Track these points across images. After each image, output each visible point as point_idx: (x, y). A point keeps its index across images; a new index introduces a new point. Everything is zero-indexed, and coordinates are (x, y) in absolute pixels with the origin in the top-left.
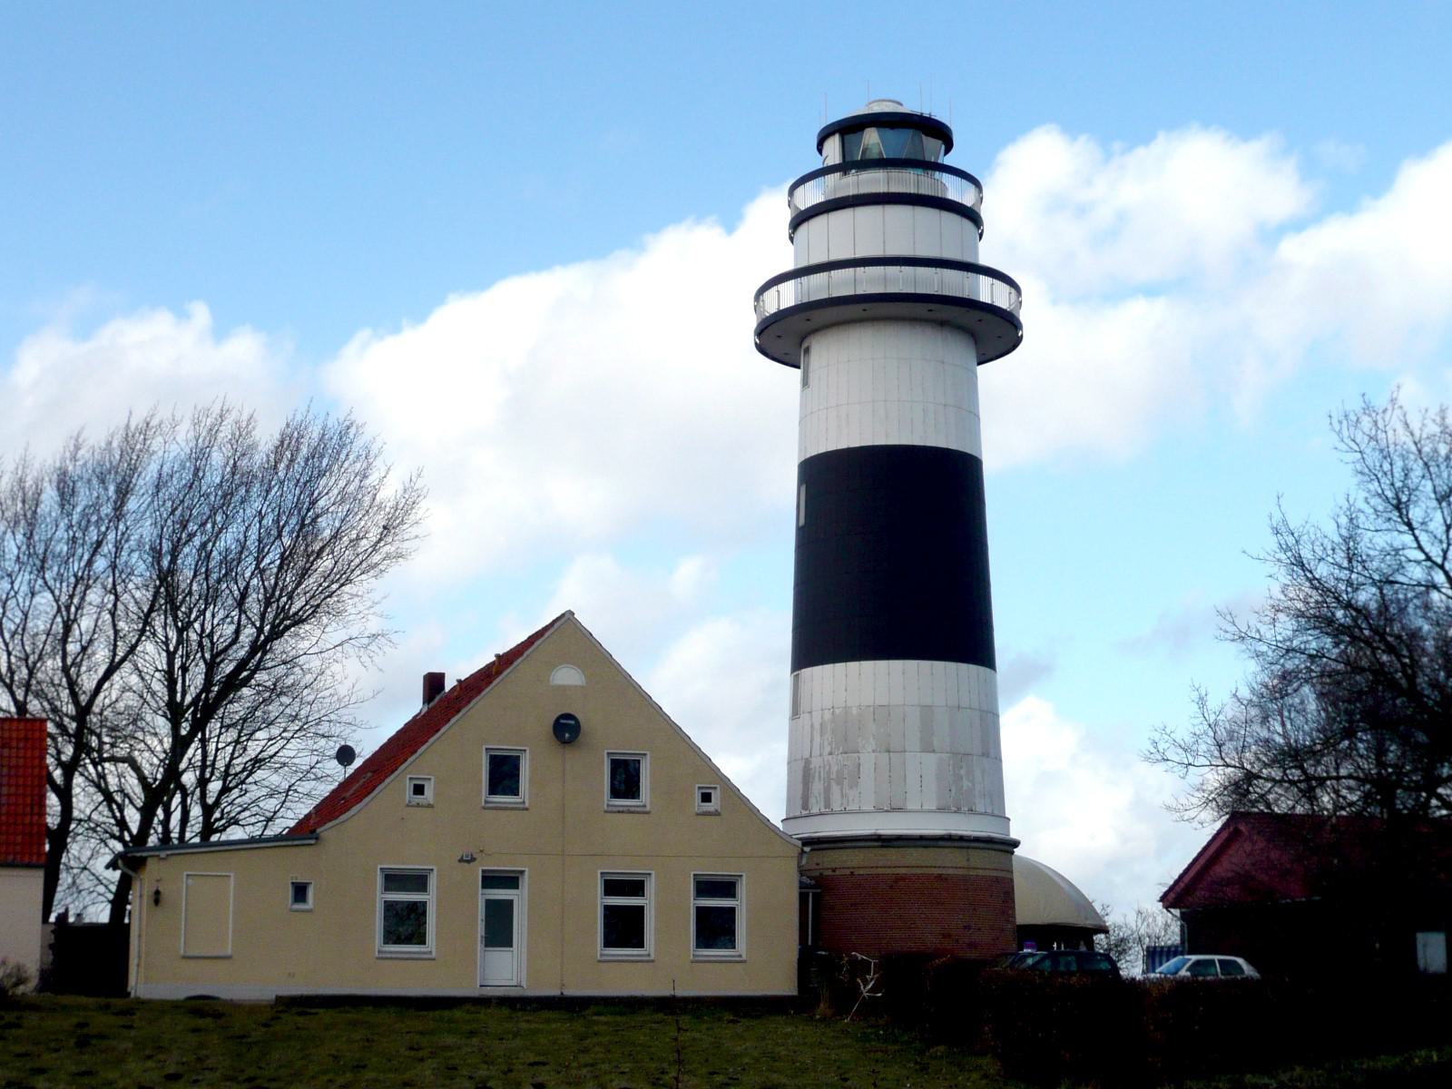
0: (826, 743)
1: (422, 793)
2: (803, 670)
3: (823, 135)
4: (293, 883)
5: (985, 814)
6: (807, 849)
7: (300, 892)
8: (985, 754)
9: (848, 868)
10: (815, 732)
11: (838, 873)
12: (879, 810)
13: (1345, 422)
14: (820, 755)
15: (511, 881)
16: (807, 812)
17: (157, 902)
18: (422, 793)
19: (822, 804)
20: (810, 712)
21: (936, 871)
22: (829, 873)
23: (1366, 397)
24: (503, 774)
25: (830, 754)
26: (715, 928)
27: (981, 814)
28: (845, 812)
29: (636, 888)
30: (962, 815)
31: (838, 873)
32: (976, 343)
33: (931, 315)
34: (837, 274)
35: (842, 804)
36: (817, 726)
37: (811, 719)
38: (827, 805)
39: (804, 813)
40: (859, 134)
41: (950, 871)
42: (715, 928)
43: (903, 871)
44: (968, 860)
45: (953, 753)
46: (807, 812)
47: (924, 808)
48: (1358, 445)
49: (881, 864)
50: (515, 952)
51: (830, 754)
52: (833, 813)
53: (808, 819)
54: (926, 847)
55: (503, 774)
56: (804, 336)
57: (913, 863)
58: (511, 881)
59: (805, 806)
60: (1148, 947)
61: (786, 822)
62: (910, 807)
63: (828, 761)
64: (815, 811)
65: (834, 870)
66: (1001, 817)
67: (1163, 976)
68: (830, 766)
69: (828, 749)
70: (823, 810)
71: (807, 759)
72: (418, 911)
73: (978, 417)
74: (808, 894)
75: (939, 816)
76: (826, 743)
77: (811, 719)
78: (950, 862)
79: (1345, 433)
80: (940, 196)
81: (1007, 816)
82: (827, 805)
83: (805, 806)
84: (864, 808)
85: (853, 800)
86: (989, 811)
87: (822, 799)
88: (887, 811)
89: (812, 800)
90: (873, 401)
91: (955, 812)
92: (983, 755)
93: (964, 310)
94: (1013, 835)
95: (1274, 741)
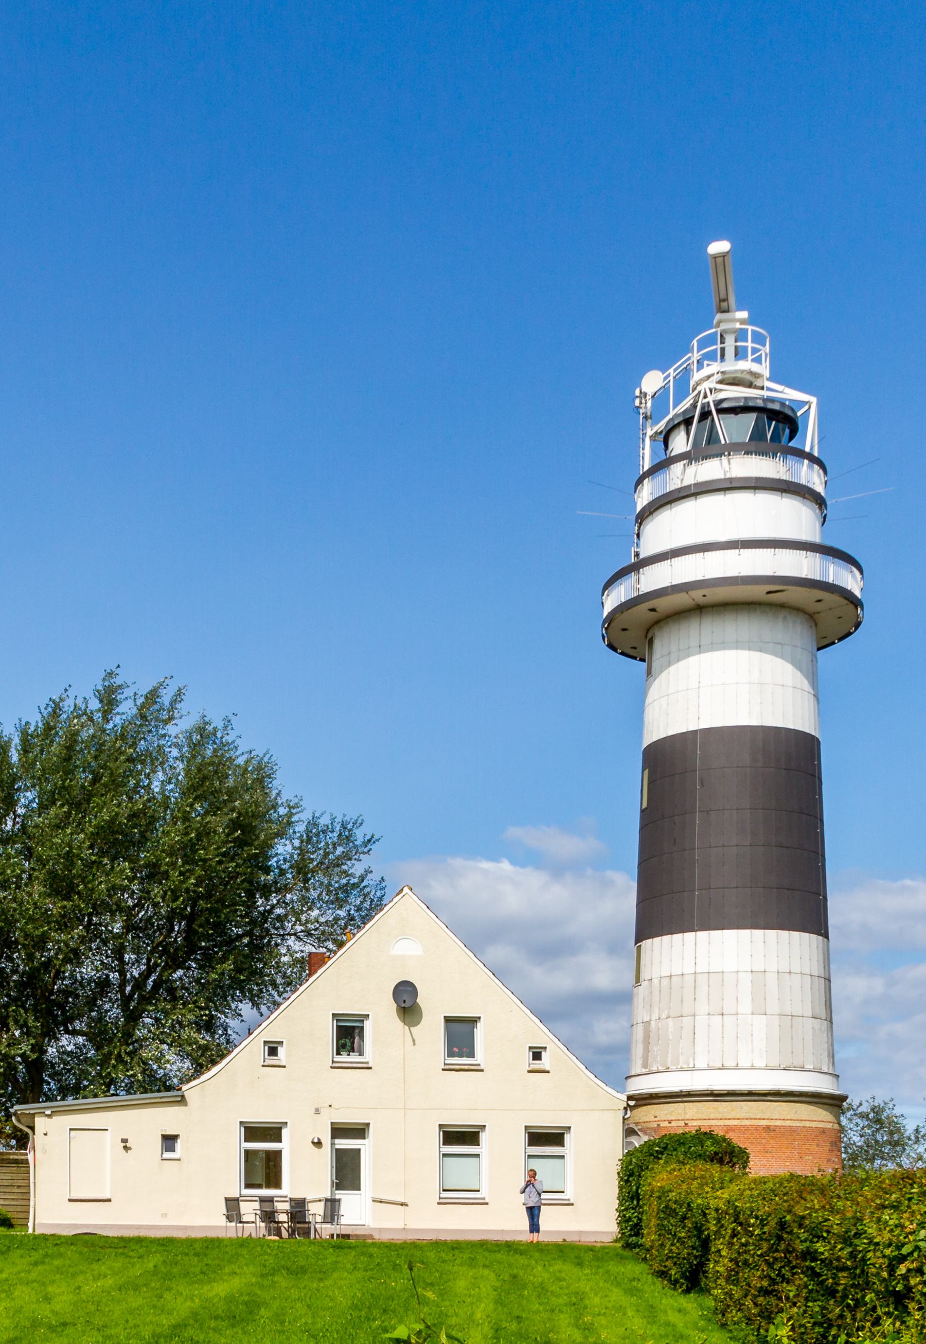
1: (540, 1059)
4: (368, 1124)
6: (632, 1103)
7: (169, 1141)
11: (674, 1124)
15: (360, 1131)
17: (126, 1148)
18: (540, 1059)
24: (348, 1035)
31: (674, 1124)
33: (703, 592)
39: (644, 1071)
41: (778, 1123)
49: (712, 1116)
50: (363, 1195)
55: (348, 1035)
57: (743, 1115)
58: (360, 1131)
60: (683, 1275)
64: (654, 1069)
72: (274, 1159)
80: (831, 581)
93: (700, 555)
95: (20, 760)
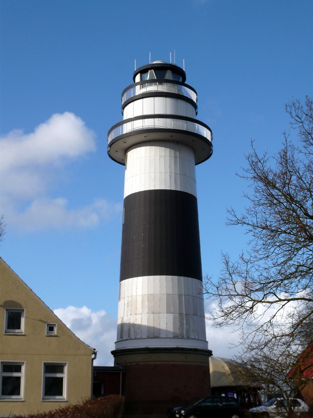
0: (129, 311)
2: (122, 281)
3: (135, 74)
5: (195, 339)
8: (195, 314)
9: (136, 362)
10: (125, 306)
12: (149, 338)
13: (293, 107)
14: (127, 316)
16: (122, 339)
19: (127, 336)
20: (124, 298)
21: (172, 363)
22: (129, 364)
23: (308, 97)
25: (131, 315)
26: (53, 387)
27: (193, 339)
28: (136, 339)
29: (18, 368)
30: (184, 339)
32: (195, 153)
34: (136, 122)
35: (135, 335)
36: (126, 304)
37: (124, 301)
38: (129, 336)
39: (121, 339)
40: (147, 73)
41: (178, 363)
42: (53, 387)
43: (158, 363)
44: (186, 358)
45: (180, 314)
46: (122, 339)
47: (167, 336)
48: (301, 119)
51: (131, 315)
52: (131, 339)
53: (122, 342)
54: (168, 353)
56: (126, 150)
59: (121, 337)
61: (117, 343)
62: (161, 336)
63: (130, 318)
64: (125, 339)
65: (131, 363)
66: (205, 341)
67: (63, 410)
68: (130, 319)
69: (130, 313)
70: (127, 338)
71: (122, 317)
73: (195, 181)
74: (120, 373)
75: (175, 339)
76: (129, 311)
77: (124, 301)
78: (179, 359)
79: (294, 114)
81: (207, 340)
82: (129, 336)
83: (121, 337)
84: (143, 337)
85: (139, 334)
86: (197, 338)
87: (127, 334)
88: (152, 338)
89: (124, 334)
90: (149, 173)
91: (181, 338)
92: (194, 315)
94: (210, 348)
